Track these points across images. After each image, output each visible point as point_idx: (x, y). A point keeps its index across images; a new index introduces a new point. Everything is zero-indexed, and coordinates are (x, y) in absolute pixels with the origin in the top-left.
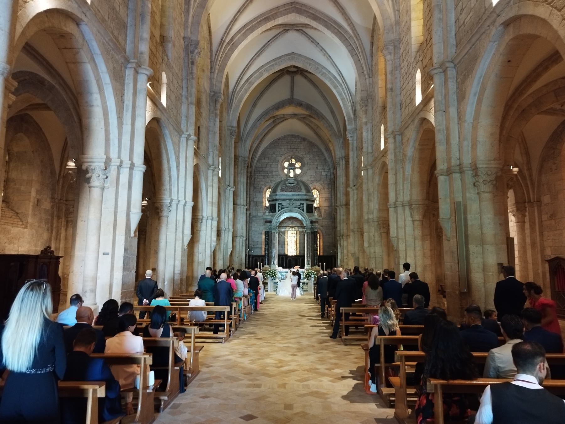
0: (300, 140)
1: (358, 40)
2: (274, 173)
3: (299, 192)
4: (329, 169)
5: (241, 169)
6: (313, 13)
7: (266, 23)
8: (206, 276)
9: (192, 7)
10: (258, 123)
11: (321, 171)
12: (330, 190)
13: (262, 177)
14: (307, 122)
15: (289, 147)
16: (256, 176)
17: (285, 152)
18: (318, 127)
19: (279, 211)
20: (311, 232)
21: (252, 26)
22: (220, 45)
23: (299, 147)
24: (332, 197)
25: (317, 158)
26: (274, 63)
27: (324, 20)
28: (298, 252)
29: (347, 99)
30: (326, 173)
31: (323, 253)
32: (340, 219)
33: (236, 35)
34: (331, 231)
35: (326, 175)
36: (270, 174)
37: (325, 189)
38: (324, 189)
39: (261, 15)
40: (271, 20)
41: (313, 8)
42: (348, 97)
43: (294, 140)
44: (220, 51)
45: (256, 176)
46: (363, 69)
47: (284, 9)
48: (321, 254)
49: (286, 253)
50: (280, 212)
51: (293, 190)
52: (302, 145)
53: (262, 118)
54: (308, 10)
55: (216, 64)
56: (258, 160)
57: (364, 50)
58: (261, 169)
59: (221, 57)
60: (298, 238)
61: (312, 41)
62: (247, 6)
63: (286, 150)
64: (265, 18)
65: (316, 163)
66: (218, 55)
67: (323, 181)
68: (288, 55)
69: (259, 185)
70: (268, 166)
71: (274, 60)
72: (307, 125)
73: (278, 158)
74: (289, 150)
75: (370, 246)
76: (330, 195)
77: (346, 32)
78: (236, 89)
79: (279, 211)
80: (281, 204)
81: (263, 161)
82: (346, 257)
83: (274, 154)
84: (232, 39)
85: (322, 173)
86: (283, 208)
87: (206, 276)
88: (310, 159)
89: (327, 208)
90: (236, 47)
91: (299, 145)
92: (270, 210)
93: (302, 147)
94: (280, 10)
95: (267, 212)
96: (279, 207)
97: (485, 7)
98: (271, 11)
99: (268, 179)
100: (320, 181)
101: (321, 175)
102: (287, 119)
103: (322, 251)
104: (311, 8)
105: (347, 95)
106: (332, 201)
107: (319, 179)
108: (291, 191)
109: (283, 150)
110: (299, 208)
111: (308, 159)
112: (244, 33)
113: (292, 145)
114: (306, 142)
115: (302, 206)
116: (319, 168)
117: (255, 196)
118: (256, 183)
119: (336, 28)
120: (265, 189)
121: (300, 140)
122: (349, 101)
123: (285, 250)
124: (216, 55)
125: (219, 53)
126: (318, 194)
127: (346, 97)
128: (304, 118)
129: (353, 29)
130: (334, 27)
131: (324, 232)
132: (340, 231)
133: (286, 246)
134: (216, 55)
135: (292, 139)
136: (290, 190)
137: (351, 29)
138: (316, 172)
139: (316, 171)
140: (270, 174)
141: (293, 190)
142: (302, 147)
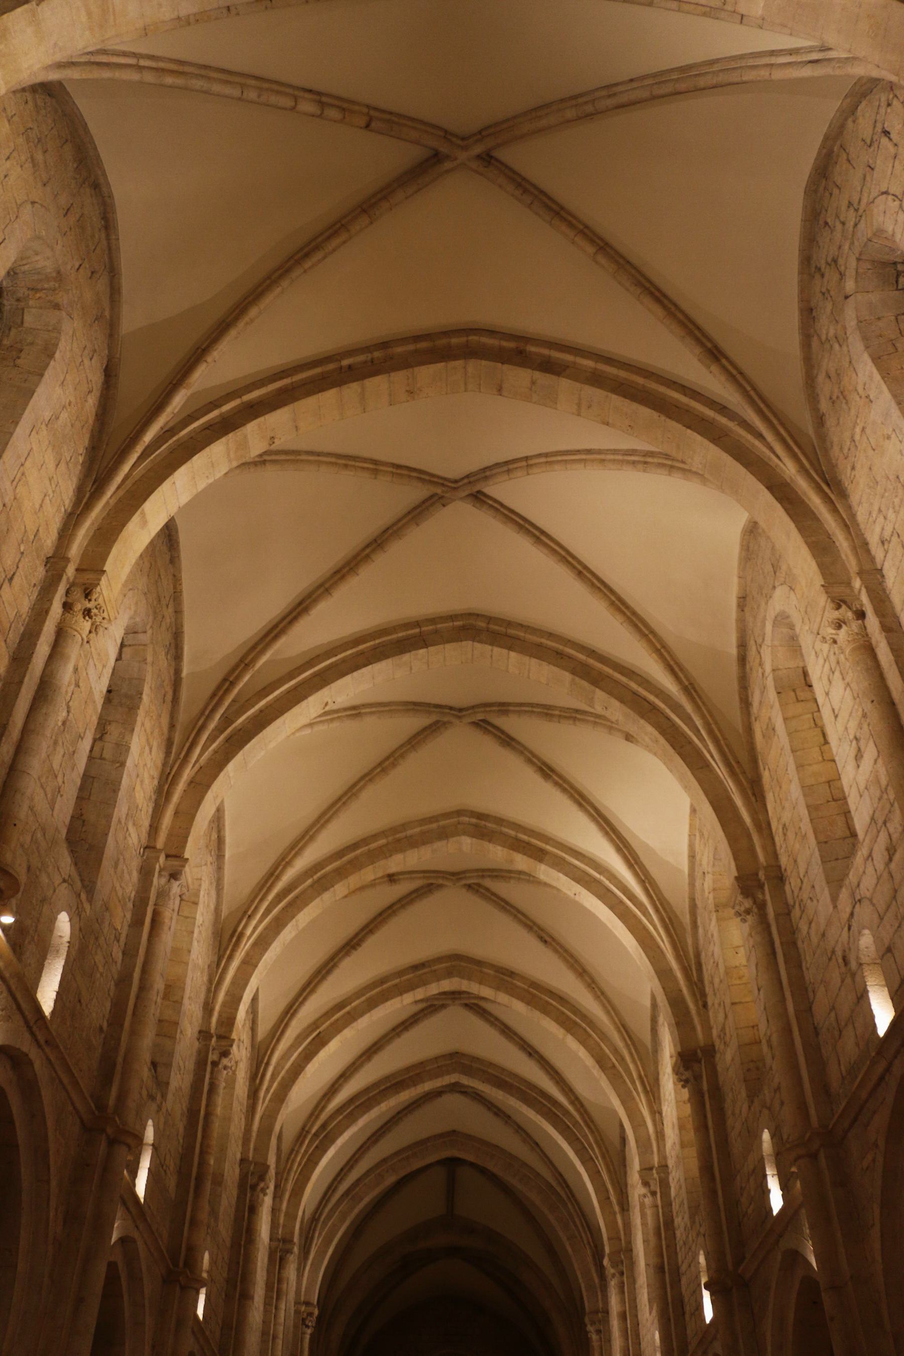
1: (592, 1132)
6: (497, 1074)
7: (398, 1093)
9: (261, 1101)
21: (369, 1099)
22: (297, 1140)
26: (410, 1152)
27: (519, 1088)
29: (581, 1237)
33: (332, 1117)
39: (387, 1078)
40: (408, 1087)
41: (495, 1065)
42: (583, 1235)
44: (298, 1152)
46: (607, 1191)
47: (436, 1066)
54: (485, 1069)
55: (287, 1180)
57: (608, 1151)
59: (299, 1164)
61: (370, 780)
62: (368, 1148)
64: (395, 1084)
66: (294, 1160)
68: (441, 1136)
71: (409, 1147)
75: (29, 943)
77: (567, 1112)
78: (321, 1214)
84: (324, 1126)
90: (333, 1141)
94: (428, 1068)
97: (814, 1024)
98: (408, 1069)
104: (491, 1064)
105: (581, 1229)
112: (351, 1113)
119: (544, 1105)
122: (585, 1242)
124: (288, 1159)
125: (296, 1156)
127: (579, 1232)
129: (582, 1110)
130: (541, 1102)
134: (288, 1159)
137: (578, 1111)
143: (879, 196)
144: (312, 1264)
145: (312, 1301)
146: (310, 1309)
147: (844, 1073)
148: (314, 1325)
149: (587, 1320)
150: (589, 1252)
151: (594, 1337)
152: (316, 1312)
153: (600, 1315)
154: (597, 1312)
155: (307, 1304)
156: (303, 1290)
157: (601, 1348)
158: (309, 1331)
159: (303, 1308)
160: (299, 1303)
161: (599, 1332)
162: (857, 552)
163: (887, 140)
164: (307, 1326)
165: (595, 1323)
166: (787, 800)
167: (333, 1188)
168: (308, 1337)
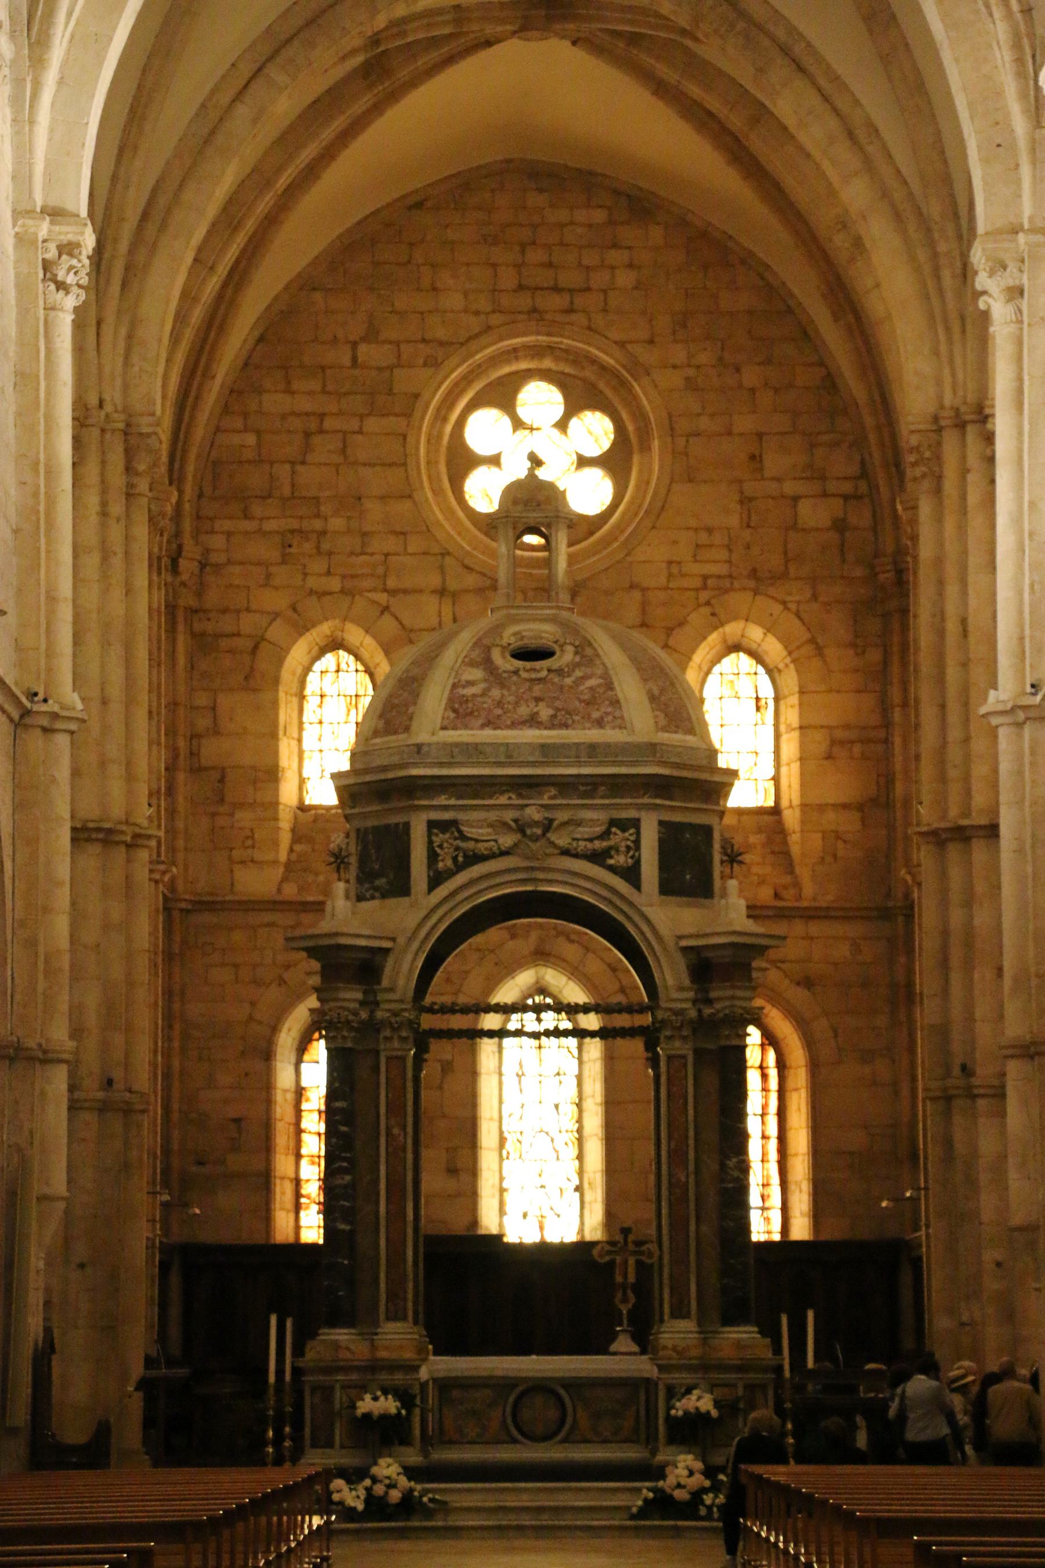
0: (599, 216)
2: (374, 510)
3: (600, 723)
4: (864, 474)
5: (104, 514)
8: (505, 1240)
10: (242, 111)
11: (790, 488)
12: (874, 656)
13: (266, 550)
14: (663, 71)
15: (508, 279)
16: (217, 542)
17: (475, 323)
18: (761, 114)
19: (435, 881)
20: (698, 1053)
23: (598, 280)
24: (887, 724)
25: (751, 376)
28: (596, 1215)
30: (836, 505)
31: (817, 1214)
32: (945, 933)
34: (882, 1021)
35: (840, 526)
36: (337, 523)
37: (831, 652)
38: (820, 651)
43: (562, 215)
45: (217, 542)
48: (801, 1230)
49: (489, 1222)
50: (442, 891)
51: (545, 712)
52: (614, 256)
53: (272, 71)
56: (235, 392)
58: (255, 479)
60: (595, 1088)
63: (483, 303)
65: (745, 423)
67: (813, 581)
69: (247, 623)
70: (324, 448)
72: (661, 89)
73: (404, 381)
74: (505, 301)
76: (869, 701)
79: (435, 881)
80: (454, 823)
81: (274, 402)
82: (997, 1255)
83: (371, 335)
85: (805, 508)
86: (476, 858)
87: (505, 1240)
88: (691, 385)
89: (849, 823)
91: (590, 258)
92: (366, 876)
93: (625, 279)
95: (340, 887)
96: (433, 856)
99: (318, 566)
100: (784, 576)
101: (793, 526)
102: (488, 44)
103: (801, 1202)
106: (887, 757)
107: (775, 561)
108: (533, 721)
109: (454, 301)
110: (597, 858)
111: (676, 379)
113: (536, 256)
114: (656, 234)
115: (618, 837)
116: (774, 462)
117: (203, 723)
118: (212, 598)
120: (298, 652)
121: (599, 216)
123: (473, 1195)
126: (767, 691)
128: (634, 39)
131: (821, 1026)
132: (942, 1031)
133: (487, 1160)
135: (535, 200)
136: (524, 711)
138: (745, 501)
139: (749, 488)
140: (337, 523)
141: (545, 712)
142: (625, 279)
143: (457, 559)
144: (61, 82)
145: (70, 207)
146: (67, 233)
147: (823, 688)
148: (85, 281)
149: (978, 256)
150: (1001, 30)
151: (999, 310)
152: (89, 240)
153: (1021, 238)
154: (1015, 230)
155: (55, 213)
156: (39, 169)
157: (1020, 343)
158: (70, 301)
159: (44, 228)
160: (29, 213)
161: (1016, 293)
162: (460, 763)
163: (504, 421)
164: (61, 286)
165: (1005, 268)
166: (442, 860)
167: (217, 322)
168: (65, 322)
